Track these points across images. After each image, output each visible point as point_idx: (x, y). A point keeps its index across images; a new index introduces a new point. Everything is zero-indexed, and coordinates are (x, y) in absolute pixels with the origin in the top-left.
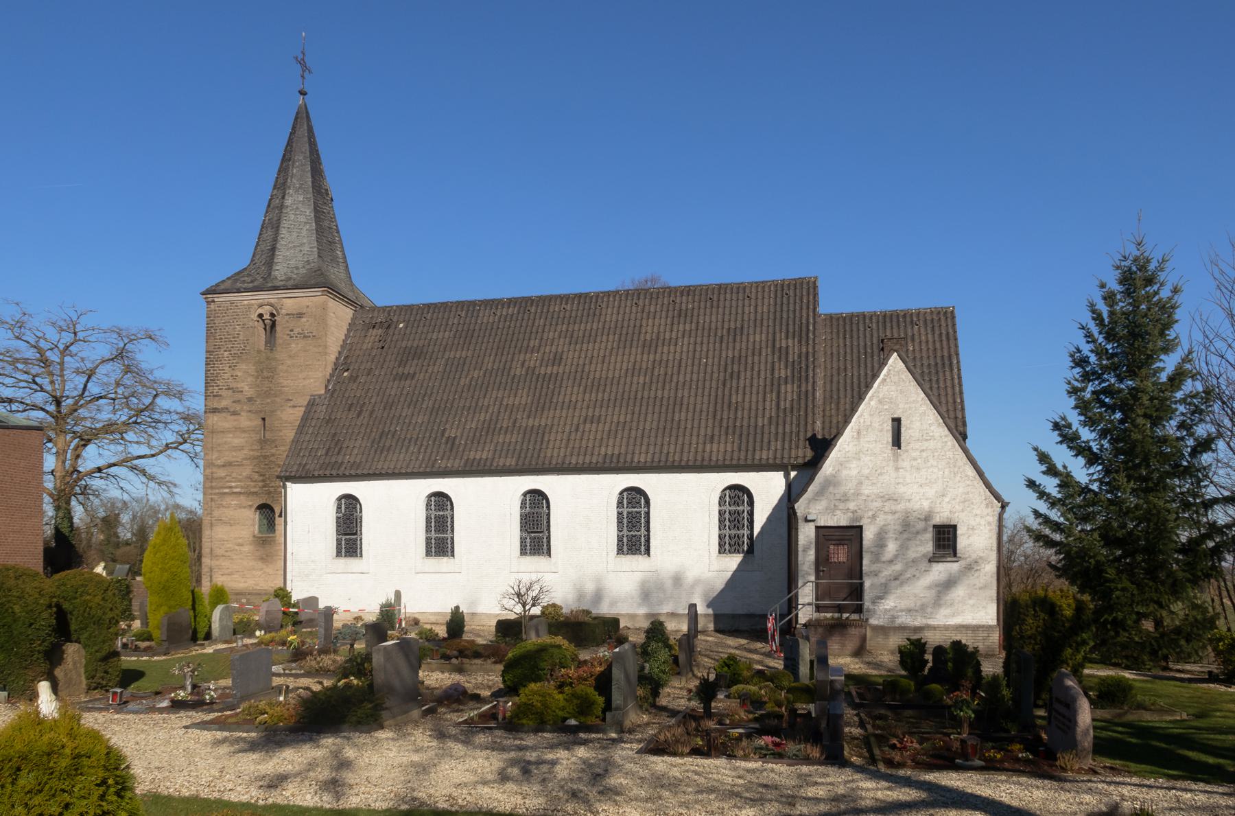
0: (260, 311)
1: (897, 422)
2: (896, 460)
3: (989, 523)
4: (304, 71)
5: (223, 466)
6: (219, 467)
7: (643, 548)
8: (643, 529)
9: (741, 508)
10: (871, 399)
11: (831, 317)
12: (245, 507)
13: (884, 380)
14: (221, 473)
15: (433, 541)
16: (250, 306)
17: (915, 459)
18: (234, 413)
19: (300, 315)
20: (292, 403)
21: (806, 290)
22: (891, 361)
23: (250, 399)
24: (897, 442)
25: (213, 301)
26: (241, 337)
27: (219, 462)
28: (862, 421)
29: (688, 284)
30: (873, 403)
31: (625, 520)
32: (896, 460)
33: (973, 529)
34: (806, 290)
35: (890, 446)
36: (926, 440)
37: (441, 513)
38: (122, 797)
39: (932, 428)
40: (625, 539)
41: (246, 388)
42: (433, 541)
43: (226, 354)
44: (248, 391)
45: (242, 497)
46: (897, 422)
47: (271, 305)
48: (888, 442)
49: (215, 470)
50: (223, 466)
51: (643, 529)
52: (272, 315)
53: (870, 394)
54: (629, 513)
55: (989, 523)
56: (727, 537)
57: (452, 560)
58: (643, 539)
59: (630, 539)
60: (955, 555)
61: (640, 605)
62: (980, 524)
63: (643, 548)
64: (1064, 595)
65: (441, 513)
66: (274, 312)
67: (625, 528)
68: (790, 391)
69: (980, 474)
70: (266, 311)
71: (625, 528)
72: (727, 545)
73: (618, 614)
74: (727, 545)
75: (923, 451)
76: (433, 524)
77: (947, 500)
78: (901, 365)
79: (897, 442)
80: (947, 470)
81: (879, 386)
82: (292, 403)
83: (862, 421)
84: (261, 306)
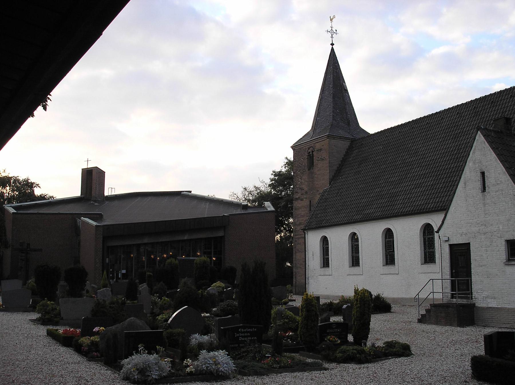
2: (484, 200)
18: (302, 200)
23: (306, 193)
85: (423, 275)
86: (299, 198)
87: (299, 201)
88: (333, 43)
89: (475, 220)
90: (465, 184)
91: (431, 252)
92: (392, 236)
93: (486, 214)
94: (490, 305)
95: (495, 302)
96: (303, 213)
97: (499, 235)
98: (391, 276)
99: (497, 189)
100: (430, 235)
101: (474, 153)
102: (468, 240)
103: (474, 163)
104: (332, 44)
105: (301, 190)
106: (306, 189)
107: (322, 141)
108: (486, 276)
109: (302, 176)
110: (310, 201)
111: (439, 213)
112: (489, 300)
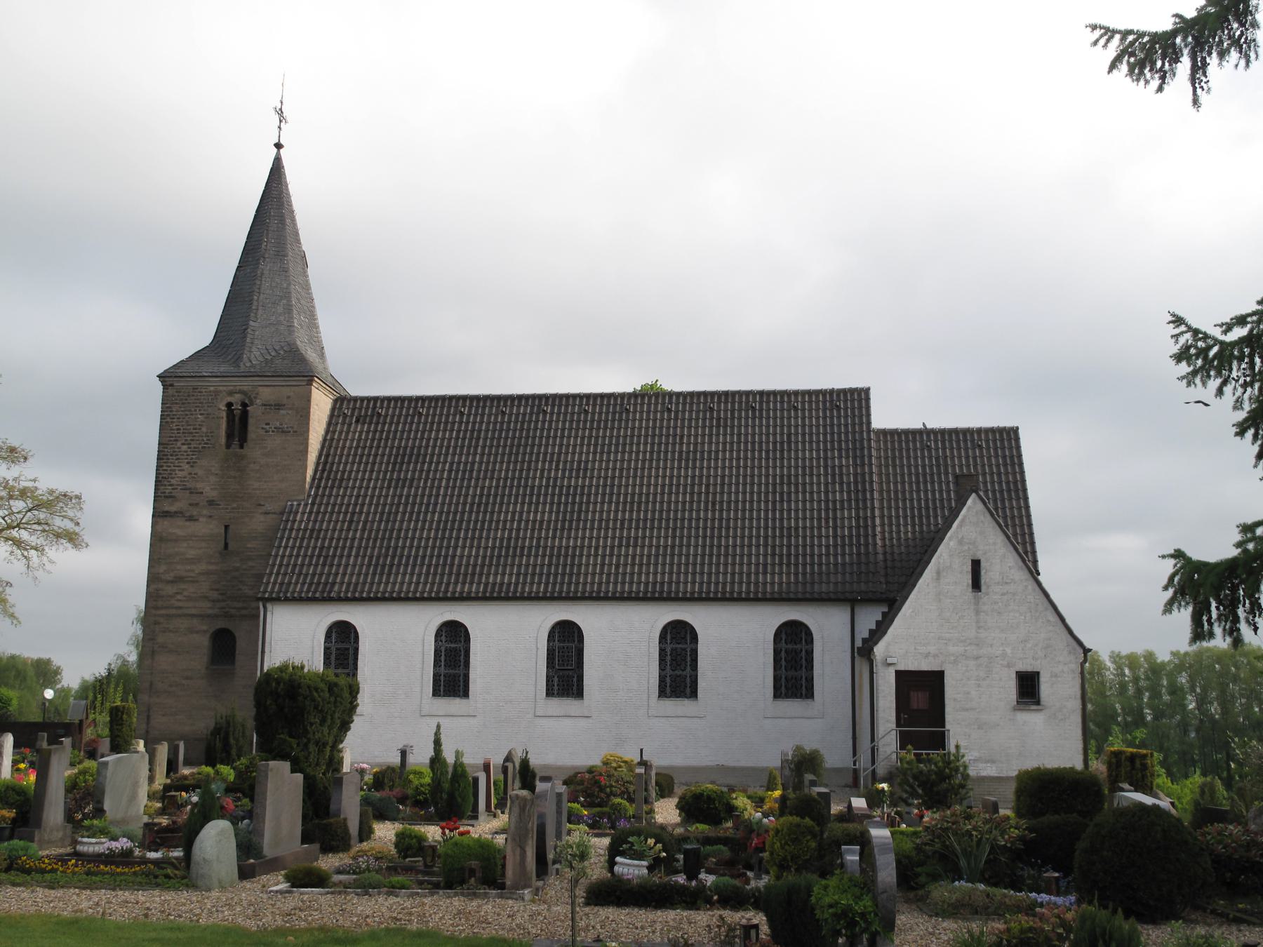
0: (229, 399)
1: (976, 565)
2: (977, 603)
3: (1073, 671)
4: (281, 121)
5: (172, 582)
6: (168, 582)
7: (688, 690)
8: (688, 668)
9: (798, 646)
10: (950, 539)
11: (884, 433)
12: (197, 632)
13: (963, 520)
14: (170, 590)
15: (442, 678)
16: (217, 393)
17: (996, 603)
18: (191, 519)
19: (279, 406)
20: (263, 509)
21: (858, 399)
22: (969, 502)
23: (211, 503)
24: (976, 584)
25: (172, 385)
26: (204, 429)
27: (169, 577)
28: (942, 561)
29: (727, 389)
30: (952, 544)
31: (668, 658)
32: (977, 603)
33: (1056, 676)
34: (858, 399)
35: (970, 590)
36: (1006, 583)
37: (453, 645)
38: (761, 835)
39: (1013, 571)
40: (668, 680)
41: (207, 489)
42: (442, 678)
43: (185, 448)
44: (209, 489)
45: (195, 621)
46: (976, 565)
47: (240, 392)
48: (968, 585)
49: (161, 586)
50: (172, 582)
51: (688, 668)
52: (244, 405)
53: (949, 534)
54: (672, 650)
55: (1073, 671)
56: (783, 679)
57: (464, 701)
58: (688, 680)
59: (674, 679)
60: (1038, 703)
61: (352, 765)
62: (1063, 671)
63: (688, 690)
64: (1022, 869)
65: (453, 645)
66: (247, 401)
67: (668, 667)
68: (848, 516)
69: (1062, 619)
70: (236, 399)
71: (668, 667)
72: (783, 688)
73: (672, 768)
74: (783, 688)
75: (1003, 594)
76: (443, 658)
77: (1029, 645)
78: (980, 506)
79: (976, 584)
80: (1028, 615)
81: (957, 527)
82: (263, 509)
83: (942, 561)
84: (231, 393)
85: (663, 720)
86: (181, 513)
87: (180, 522)
88: (281, 142)
89: (956, 635)
90: (938, 573)
91: (678, 676)
92: (804, 646)
93: (979, 628)
94: (984, 773)
95: (994, 768)
96: (192, 553)
97: (1005, 663)
98: (567, 721)
99: (1005, 591)
100: (679, 644)
101: (960, 526)
102: (941, 666)
103: (961, 542)
104: (278, 146)
105: (191, 493)
106: (213, 494)
107: (287, 386)
108: (976, 727)
109: (196, 458)
110: (226, 527)
111: (736, 603)
112: (981, 765)
